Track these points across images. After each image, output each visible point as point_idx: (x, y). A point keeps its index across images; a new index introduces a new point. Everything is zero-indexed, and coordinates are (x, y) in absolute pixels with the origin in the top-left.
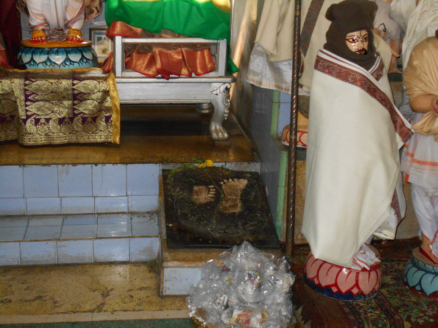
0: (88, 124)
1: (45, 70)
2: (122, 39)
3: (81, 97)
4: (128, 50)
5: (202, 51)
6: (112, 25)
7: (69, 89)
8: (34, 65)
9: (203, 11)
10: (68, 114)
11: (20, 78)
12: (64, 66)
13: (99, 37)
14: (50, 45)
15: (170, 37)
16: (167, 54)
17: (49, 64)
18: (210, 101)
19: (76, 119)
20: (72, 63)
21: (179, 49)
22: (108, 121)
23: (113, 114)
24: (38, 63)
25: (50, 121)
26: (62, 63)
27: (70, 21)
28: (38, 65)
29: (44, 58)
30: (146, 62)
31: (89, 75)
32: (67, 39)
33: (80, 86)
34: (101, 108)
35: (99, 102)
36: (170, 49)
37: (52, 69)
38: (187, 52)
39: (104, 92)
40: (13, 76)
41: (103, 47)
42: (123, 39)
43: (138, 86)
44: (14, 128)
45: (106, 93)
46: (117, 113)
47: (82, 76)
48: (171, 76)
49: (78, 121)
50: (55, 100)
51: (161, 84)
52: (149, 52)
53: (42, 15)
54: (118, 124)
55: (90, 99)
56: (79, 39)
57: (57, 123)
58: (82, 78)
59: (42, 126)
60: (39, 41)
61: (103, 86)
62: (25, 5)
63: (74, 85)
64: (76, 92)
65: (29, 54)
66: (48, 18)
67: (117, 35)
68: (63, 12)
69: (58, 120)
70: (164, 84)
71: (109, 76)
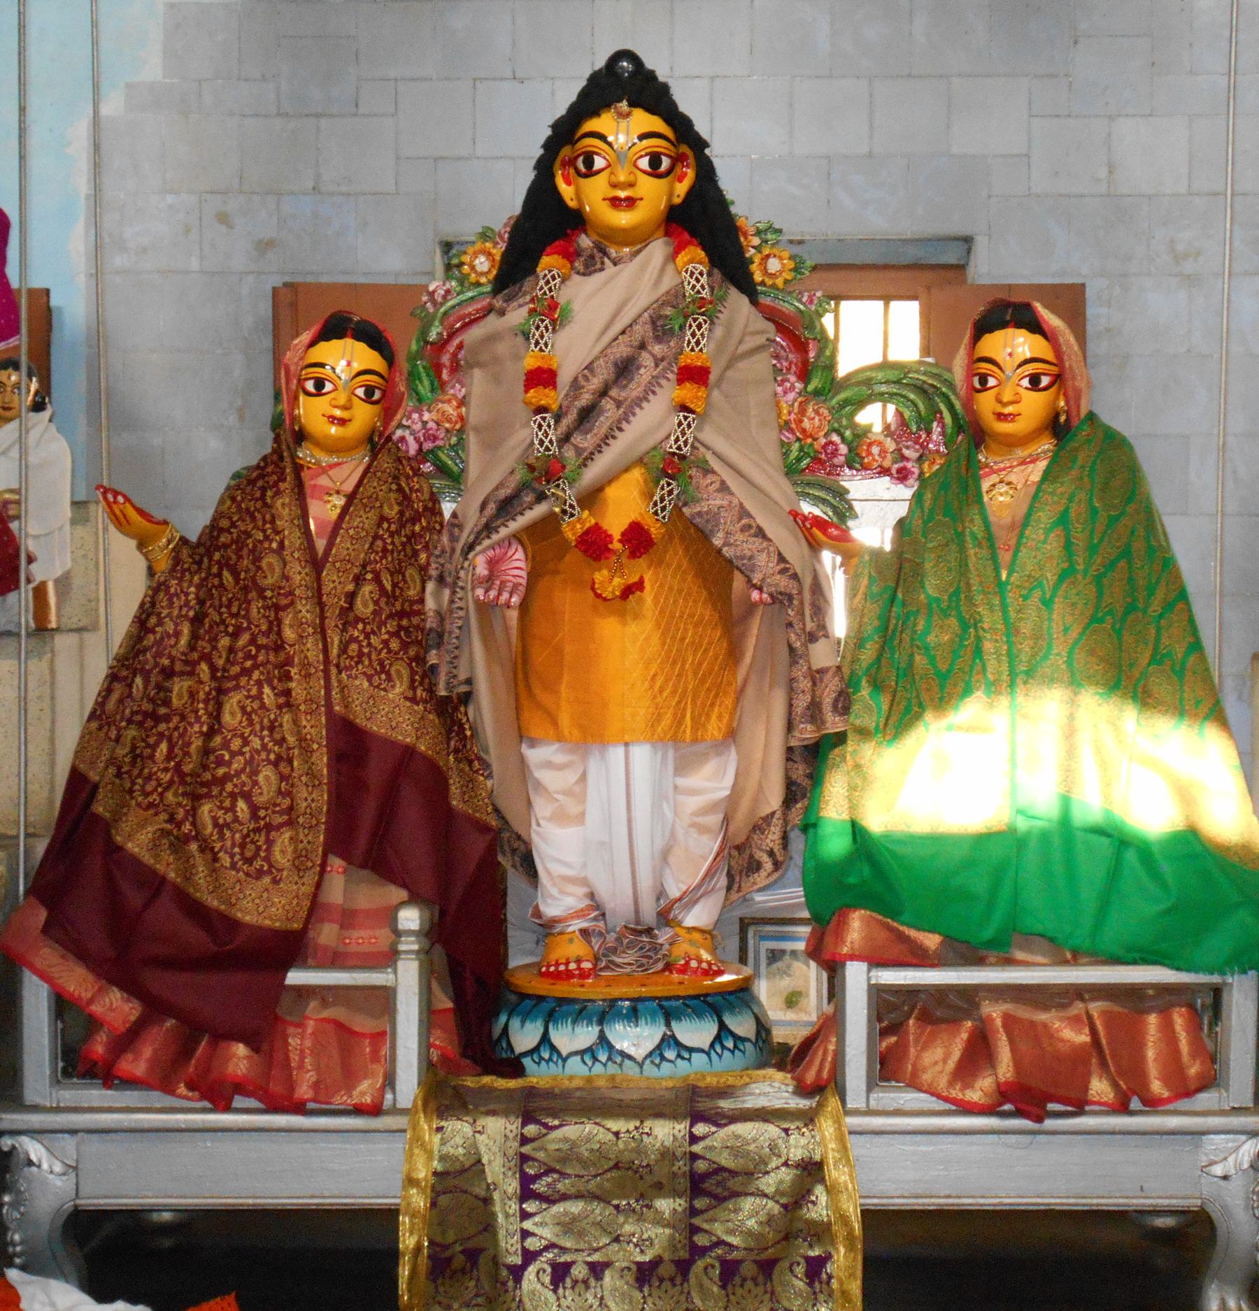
0: (742, 1286)
1: (589, 1080)
2: (869, 971)
3: (718, 1184)
4: (891, 1010)
5: (1165, 1012)
6: (833, 923)
7: (679, 1153)
8: (550, 1059)
9: (1168, 870)
10: (672, 1246)
11: (506, 1114)
12: (658, 1066)
13: (773, 951)
14: (608, 990)
15: (1040, 959)
16: (1032, 1024)
17: (603, 1057)
18: (1199, 1202)
19: (700, 1264)
20: (686, 1055)
21: (1078, 1008)
22: (818, 1274)
23: (838, 1251)
24: (564, 1054)
25: (608, 1276)
26: (651, 1054)
27: (680, 899)
28: (565, 1060)
29: (585, 1035)
30: (956, 1054)
31: (751, 1103)
32: (668, 967)
33: (718, 1142)
34: (792, 1223)
35: (785, 1206)
36: (1046, 1008)
37: (613, 1077)
38: (1108, 1017)
39: (804, 1169)
40: (482, 1109)
41: (786, 984)
42: (873, 973)
43: (925, 1146)
44: (477, 1295)
45: (812, 1170)
46: (850, 1248)
47: (725, 1104)
48: (1052, 1106)
49: (705, 1271)
50: (625, 1197)
51: (1013, 1139)
52: (968, 1015)
53: (584, 882)
54: (855, 1287)
55: (752, 1194)
56: (710, 964)
57: (632, 1281)
58: (723, 1116)
59: (577, 1290)
60: (568, 975)
61: (798, 1146)
62: (522, 848)
63: (694, 1139)
64: (701, 1166)
65: (534, 1020)
66: (604, 893)
67: (853, 957)
68: (654, 871)
69: (634, 1268)
70: (1028, 1138)
71: (820, 1105)
